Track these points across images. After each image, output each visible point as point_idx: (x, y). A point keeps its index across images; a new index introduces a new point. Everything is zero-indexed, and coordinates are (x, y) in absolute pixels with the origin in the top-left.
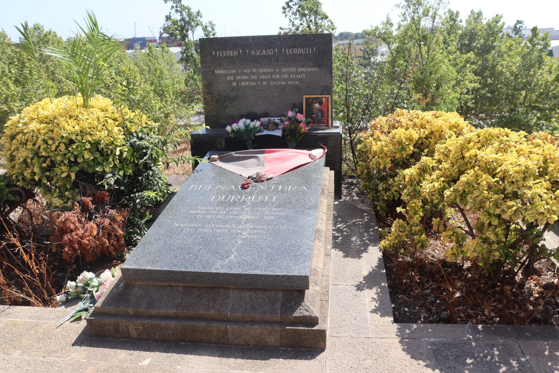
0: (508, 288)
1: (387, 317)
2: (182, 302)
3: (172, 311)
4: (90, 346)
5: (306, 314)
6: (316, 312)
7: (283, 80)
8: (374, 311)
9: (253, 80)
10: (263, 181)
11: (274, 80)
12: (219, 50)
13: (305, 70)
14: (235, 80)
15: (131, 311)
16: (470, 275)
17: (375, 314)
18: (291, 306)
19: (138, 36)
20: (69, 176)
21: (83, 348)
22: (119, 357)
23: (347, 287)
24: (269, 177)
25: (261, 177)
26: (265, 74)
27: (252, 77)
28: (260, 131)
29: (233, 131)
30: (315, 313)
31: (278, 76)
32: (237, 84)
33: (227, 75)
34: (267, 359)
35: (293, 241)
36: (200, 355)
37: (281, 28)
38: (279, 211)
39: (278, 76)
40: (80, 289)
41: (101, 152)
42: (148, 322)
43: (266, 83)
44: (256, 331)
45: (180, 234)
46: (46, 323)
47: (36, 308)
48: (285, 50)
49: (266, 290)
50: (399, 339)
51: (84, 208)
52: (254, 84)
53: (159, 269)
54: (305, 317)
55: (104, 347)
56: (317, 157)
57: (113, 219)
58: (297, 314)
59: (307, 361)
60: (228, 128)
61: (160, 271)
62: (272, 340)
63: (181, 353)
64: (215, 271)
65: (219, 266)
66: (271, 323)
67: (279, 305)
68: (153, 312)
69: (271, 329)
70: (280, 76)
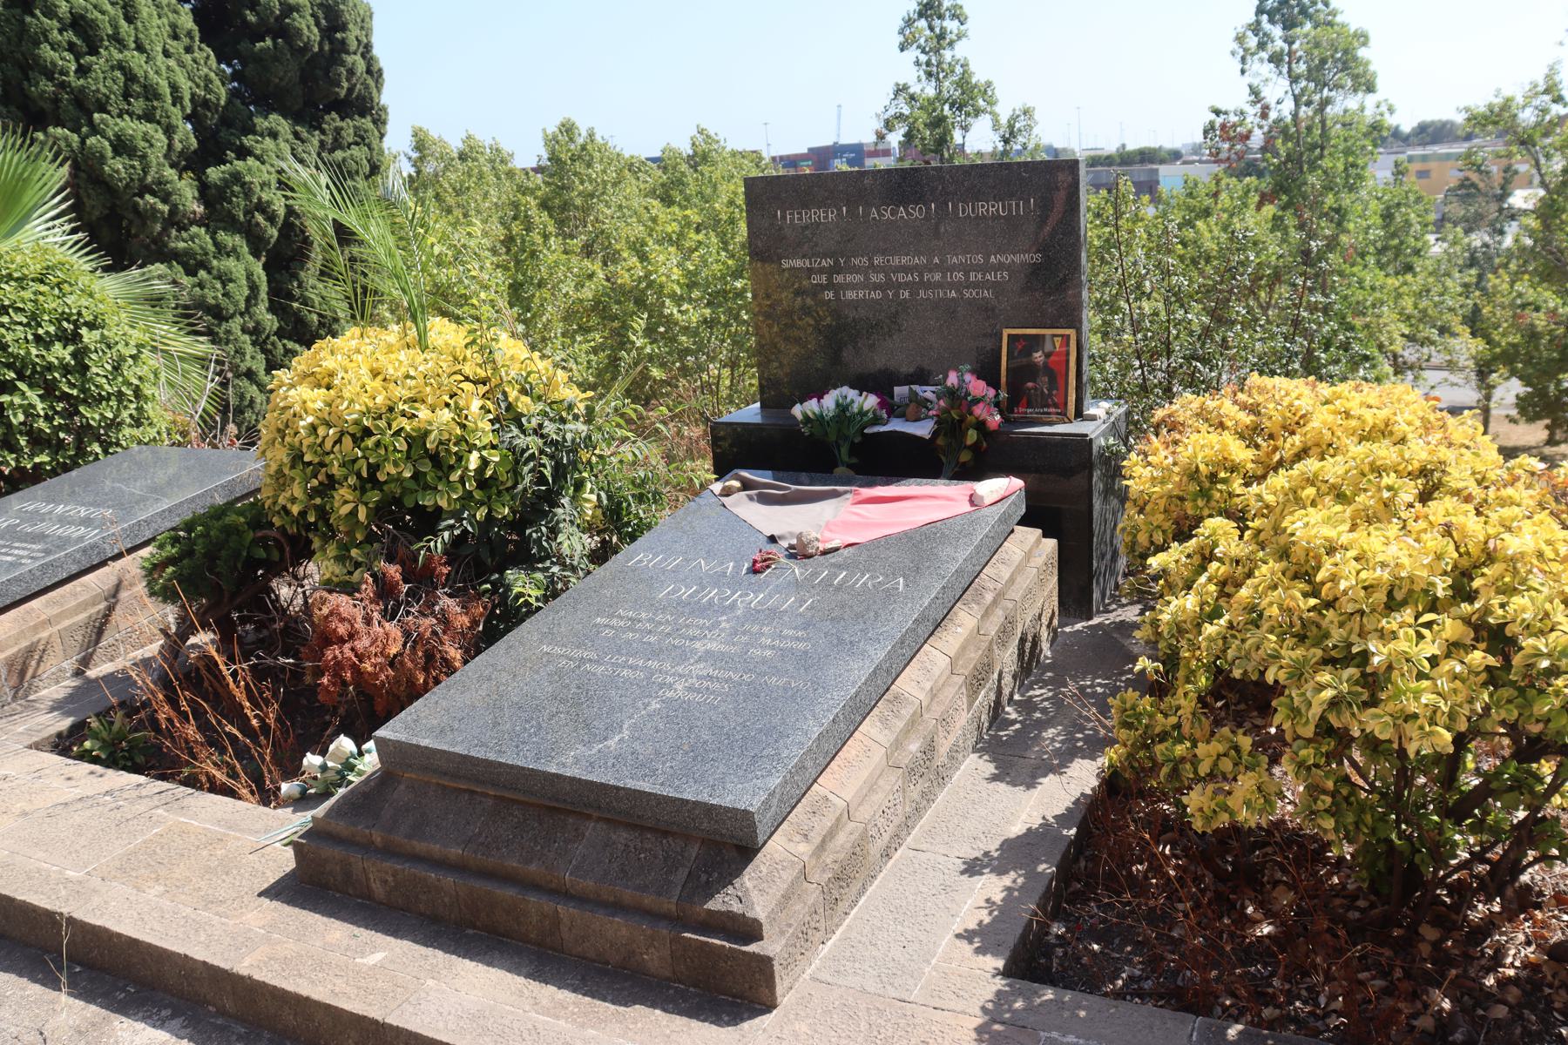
0: (1429, 933)
1: (989, 958)
2: (480, 833)
3: (455, 852)
4: (288, 903)
5: (736, 907)
6: (760, 909)
7: (952, 286)
8: (968, 936)
9: (876, 287)
10: (811, 556)
11: (928, 286)
12: (791, 207)
13: (1008, 259)
14: (830, 285)
15: (377, 838)
16: (1336, 880)
17: (964, 944)
18: (708, 882)
19: (846, 140)
20: (354, 513)
21: (276, 904)
22: (329, 938)
23: (942, 859)
24: (829, 546)
25: (805, 546)
26: (906, 269)
27: (874, 278)
28: (877, 421)
29: (807, 419)
30: (758, 908)
31: (937, 277)
32: (837, 294)
33: (810, 271)
34: (626, 1005)
35: (776, 721)
36: (489, 964)
37: (1217, 112)
38: (797, 639)
39: (937, 277)
40: (331, 775)
41: (434, 459)
42: (407, 869)
43: (907, 294)
44: (618, 929)
45: (537, 672)
46: (239, 839)
47: (246, 804)
48: (955, 207)
49: (666, 834)
50: (979, 1021)
51: (385, 590)
52: (877, 295)
53: (445, 748)
54: (730, 915)
55: (314, 910)
56: (987, 502)
57: (445, 620)
58: (715, 904)
59: (714, 1027)
60: (797, 411)
61: (444, 752)
62: (654, 959)
63: (453, 953)
64: (553, 769)
65: (572, 760)
66: (654, 916)
67: (682, 874)
68: (420, 846)
69: (649, 932)
70: (945, 276)
